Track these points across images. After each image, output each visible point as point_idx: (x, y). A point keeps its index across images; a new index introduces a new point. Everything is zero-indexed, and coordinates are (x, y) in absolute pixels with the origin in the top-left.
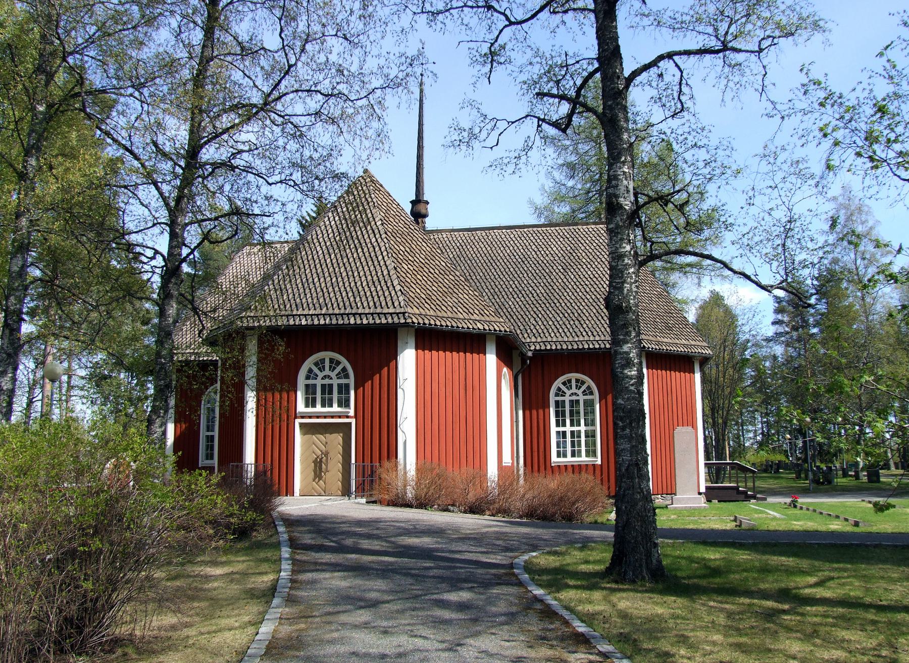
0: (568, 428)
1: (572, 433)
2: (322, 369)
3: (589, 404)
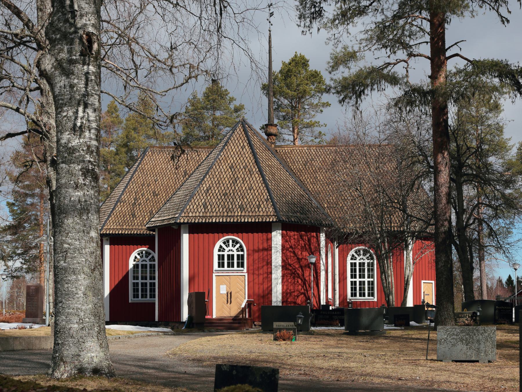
0: (358, 280)
1: (364, 277)
2: (228, 246)
3: (371, 265)
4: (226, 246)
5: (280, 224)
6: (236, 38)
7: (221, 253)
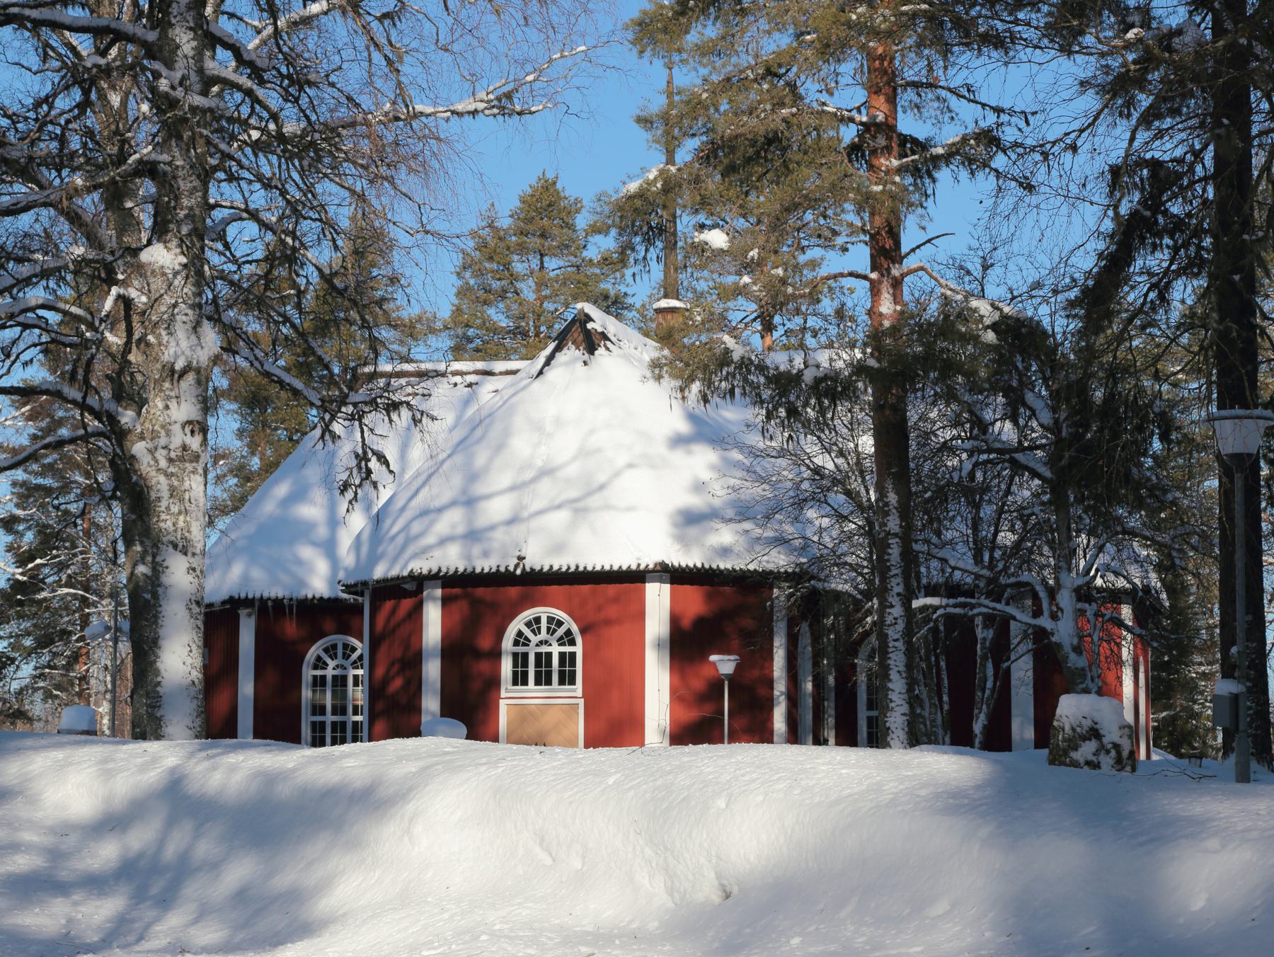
4: (533, 631)
5: (668, 575)
6: (425, 85)
7: (521, 649)
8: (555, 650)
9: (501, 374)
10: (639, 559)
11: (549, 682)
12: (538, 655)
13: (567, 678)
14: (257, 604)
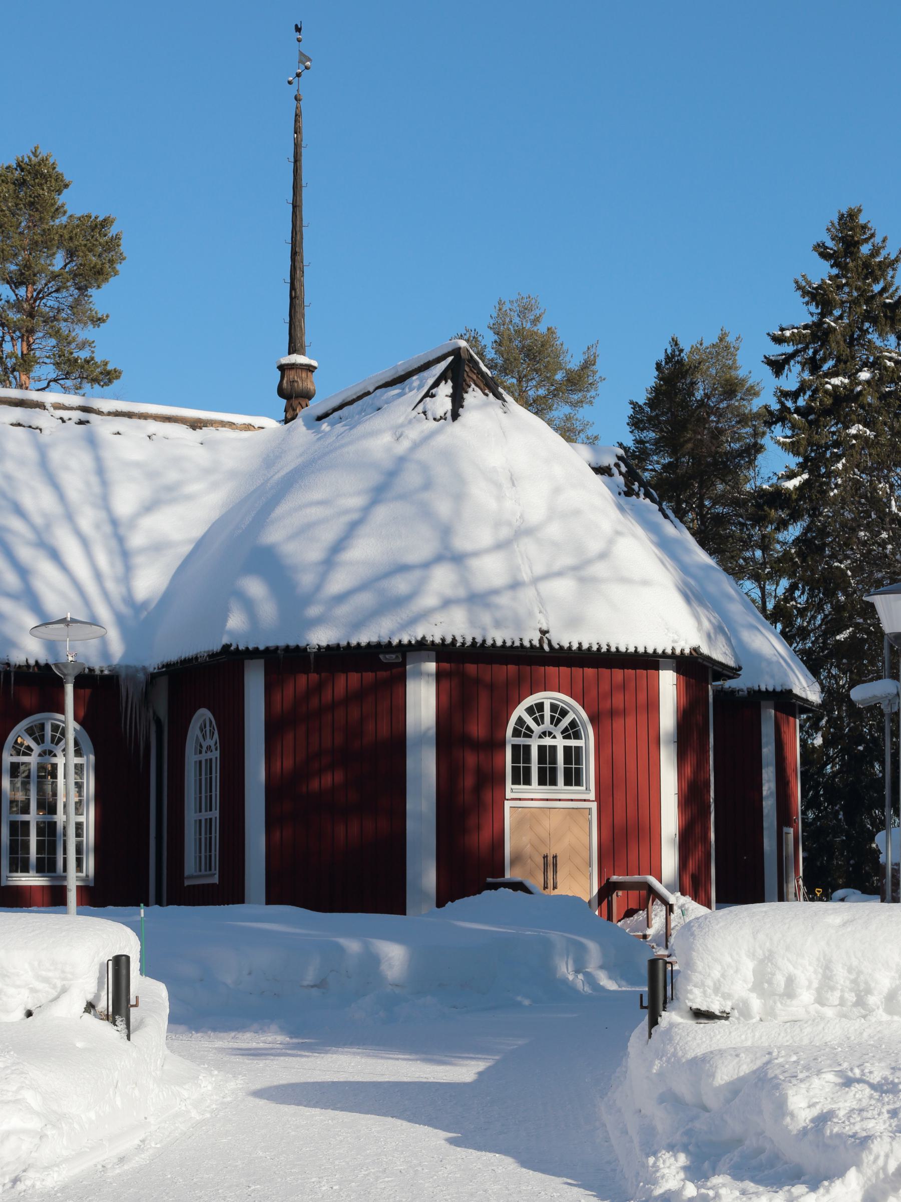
8: (560, 743)
9: (109, 414)
10: (674, 641)
11: (554, 782)
12: (541, 749)
13: (573, 778)
14: (797, 711)
